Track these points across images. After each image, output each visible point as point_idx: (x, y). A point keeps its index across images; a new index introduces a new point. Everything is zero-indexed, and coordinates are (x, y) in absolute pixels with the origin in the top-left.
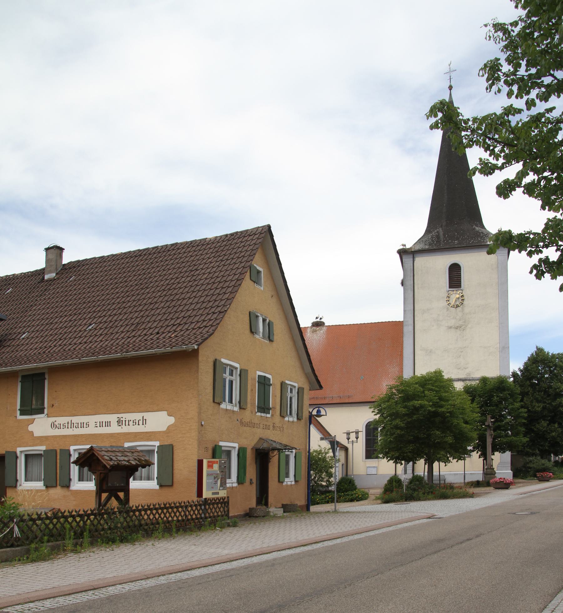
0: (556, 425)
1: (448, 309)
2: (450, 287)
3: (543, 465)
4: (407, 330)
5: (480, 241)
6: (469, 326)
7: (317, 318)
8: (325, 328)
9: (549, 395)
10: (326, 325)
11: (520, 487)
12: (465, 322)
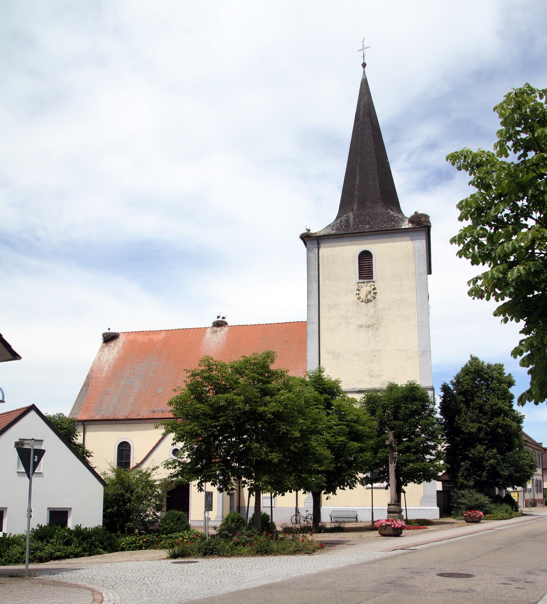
0: (495, 451)
1: (358, 305)
2: (360, 278)
3: (477, 500)
4: (312, 328)
5: (394, 225)
6: (383, 324)
7: (218, 317)
8: (226, 329)
9: (485, 414)
10: (229, 325)
11: (433, 531)
12: (378, 320)
